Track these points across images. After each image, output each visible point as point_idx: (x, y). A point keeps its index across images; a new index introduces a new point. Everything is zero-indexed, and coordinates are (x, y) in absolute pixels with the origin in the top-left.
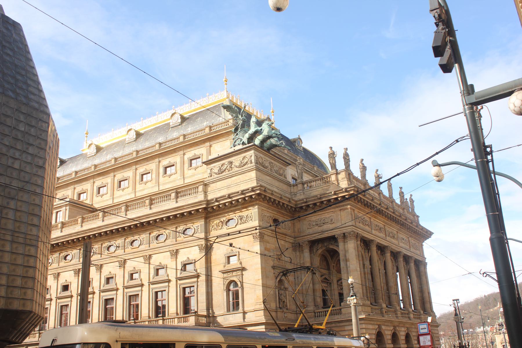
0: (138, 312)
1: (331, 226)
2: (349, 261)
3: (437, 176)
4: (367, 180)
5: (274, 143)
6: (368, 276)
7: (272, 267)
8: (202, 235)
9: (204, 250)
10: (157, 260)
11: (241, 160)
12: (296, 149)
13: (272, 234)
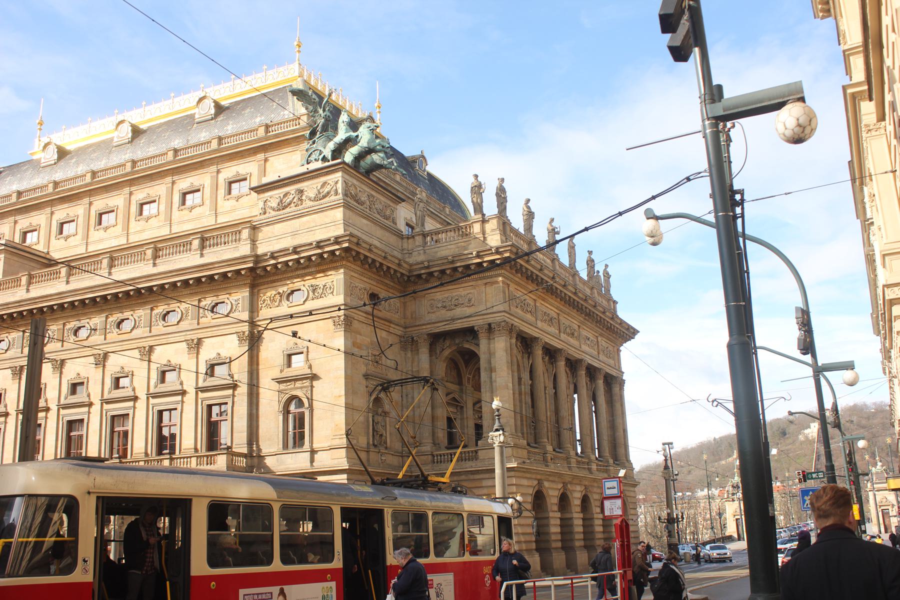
0: (127, 445)
1: (468, 311)
2: (495, 371)
3: (652, 235)
4: (534, 236)
5: (378, 162)
6: (525, 397)
7: (364, 376)
8: (245, 316)
9: (247, 341)
10: (162, 355)
11: (319, 188)
12: (415, 175)
13: (367, 320)
